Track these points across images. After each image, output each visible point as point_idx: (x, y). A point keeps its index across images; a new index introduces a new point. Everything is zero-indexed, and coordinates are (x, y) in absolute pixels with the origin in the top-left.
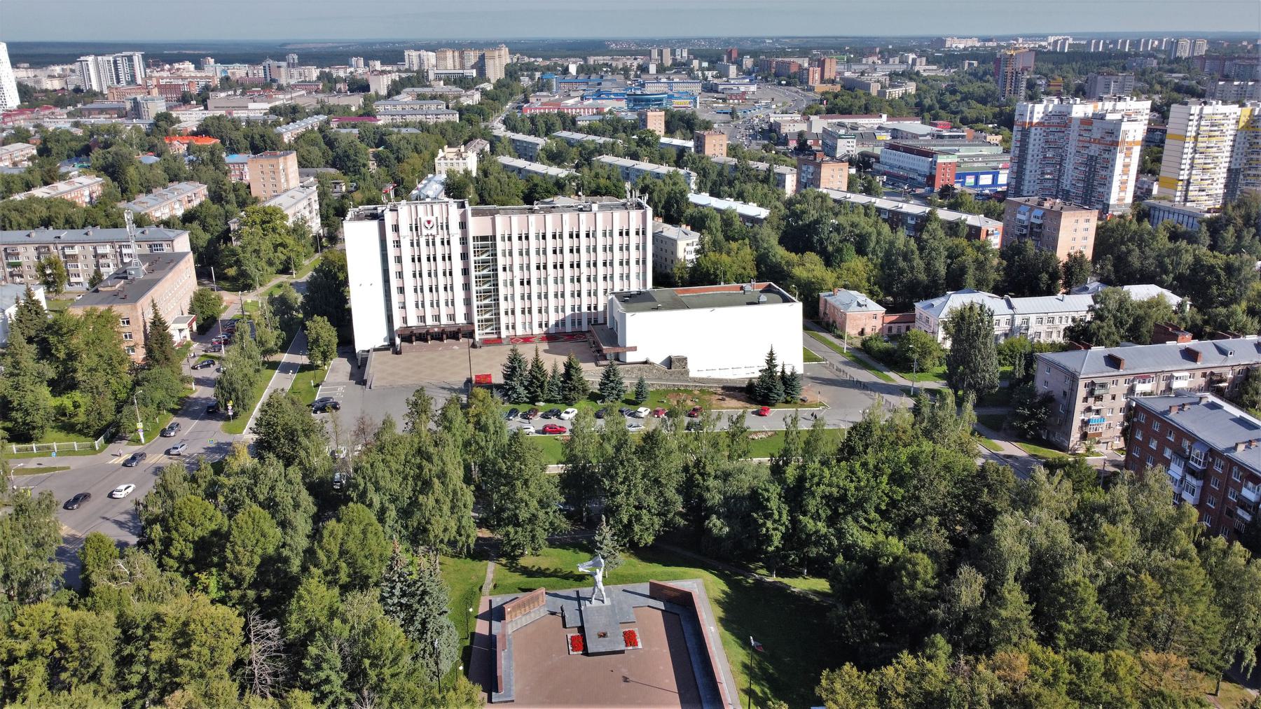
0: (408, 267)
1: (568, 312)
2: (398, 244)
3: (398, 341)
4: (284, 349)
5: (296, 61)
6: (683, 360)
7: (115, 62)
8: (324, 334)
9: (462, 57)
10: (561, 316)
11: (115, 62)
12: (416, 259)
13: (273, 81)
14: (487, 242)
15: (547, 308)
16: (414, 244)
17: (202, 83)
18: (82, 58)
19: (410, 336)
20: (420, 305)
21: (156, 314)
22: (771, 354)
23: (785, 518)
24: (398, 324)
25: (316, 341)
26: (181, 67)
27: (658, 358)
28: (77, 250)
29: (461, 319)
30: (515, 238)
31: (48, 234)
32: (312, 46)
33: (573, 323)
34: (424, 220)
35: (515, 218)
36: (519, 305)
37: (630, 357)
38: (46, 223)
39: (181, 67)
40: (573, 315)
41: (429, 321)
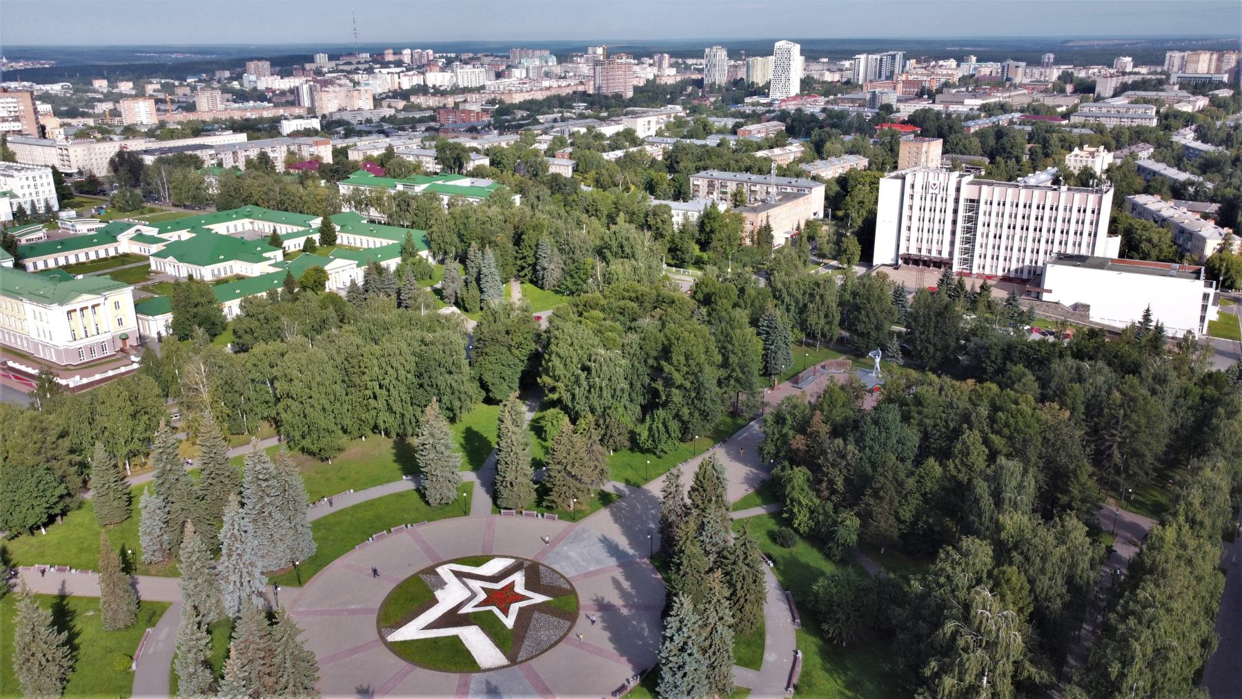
0: (916, 213)
1: (1027, 263)
2: (912, 197)
3: (900, 262)
4: (834, 258)
5: (1052, 60)
6: (1087, 307)
7: (881, 60)
8: (851, 247)
9: (1219, 60)
10: (1020, 265)
11: (881, 60)
12: (923, 209)
13: (1008, 79)
14: (974, 203)
15: (1011, 258)
16: (922, 198)
17: (943, 80)
18: (857, 56)
19: (908, 260)
20: (921, 240)
21: (768, 222)
22: (1148, 310)
23: (999, 361)
24: (902, 251)
25: (845, 251)
26: (945, 64)
27: (1067, 302)
28: (757, 188)
29: (945, 255)
30: (995, 203)
31: (744, 176)
32: (1096, 43)
33: (1029, 273)
34: (932, 182)
35: (997, 190)
36: (990, 252)
37: (1046, 297)
38: (748, 169)
39: (945, 64)
40: (1030, 267)
41: (924, 253)
